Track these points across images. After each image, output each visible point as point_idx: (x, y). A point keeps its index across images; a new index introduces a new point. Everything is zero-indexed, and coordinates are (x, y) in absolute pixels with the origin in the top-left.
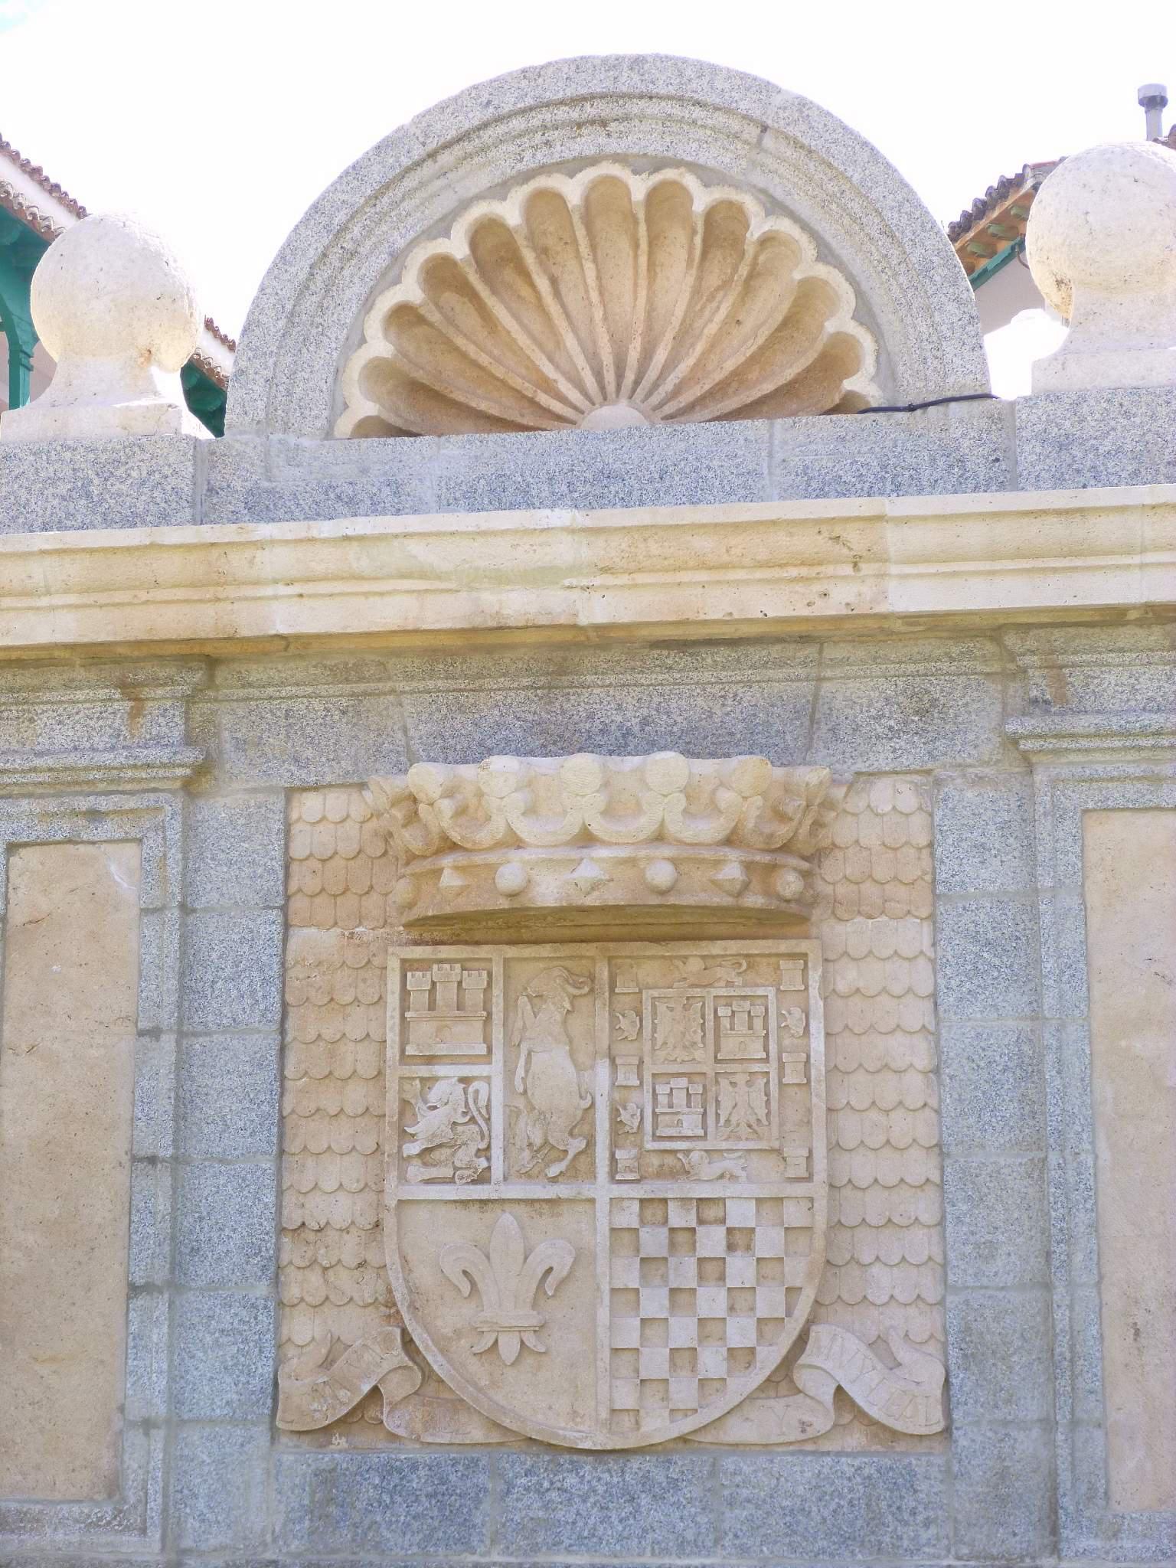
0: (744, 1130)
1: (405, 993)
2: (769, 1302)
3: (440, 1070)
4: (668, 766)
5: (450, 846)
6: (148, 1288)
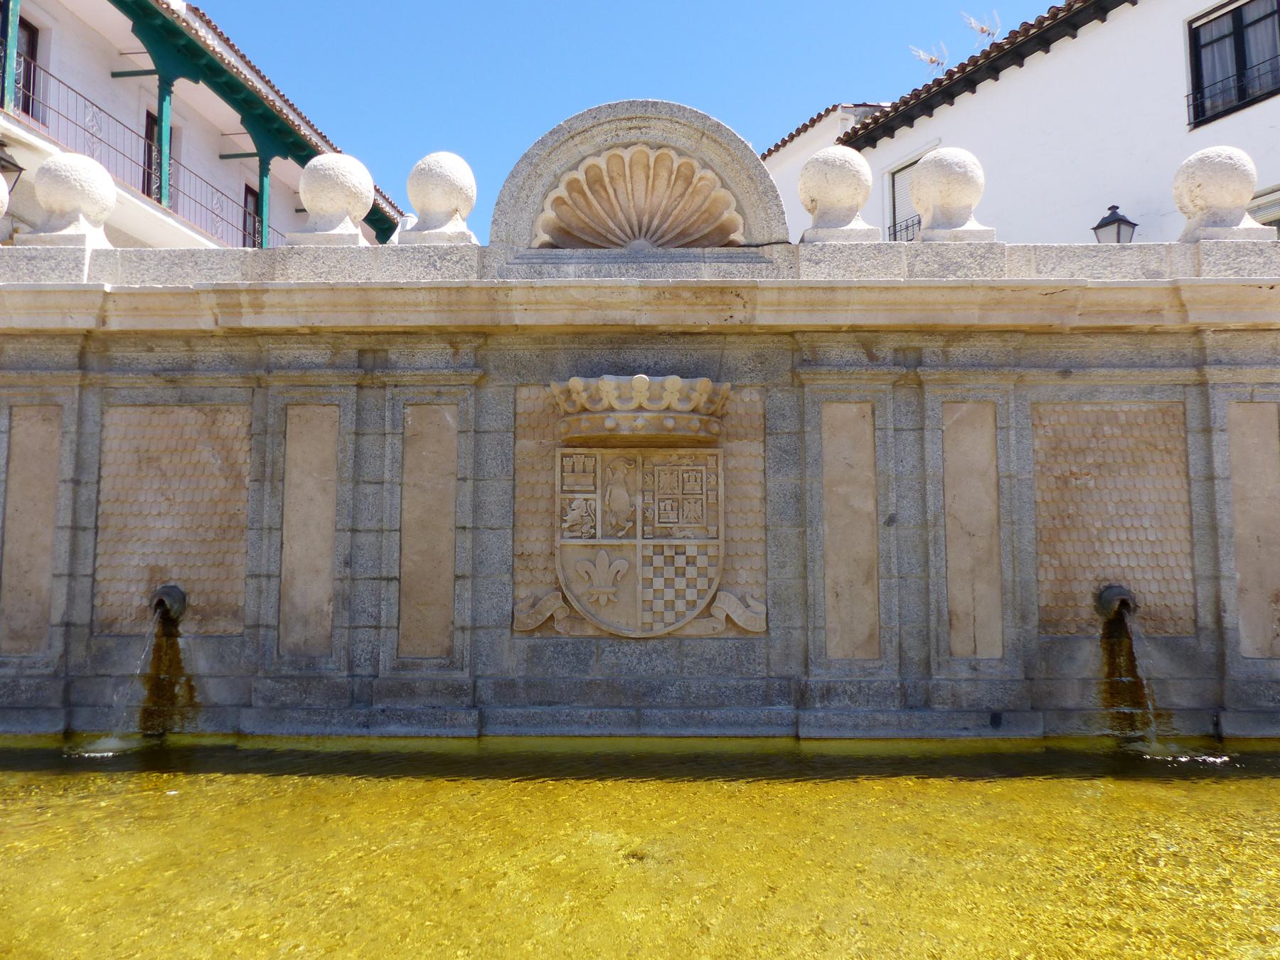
0: (693, 520)
1: (562, 466)
2: (702, 583)
3: (577, 496)
4: (673, 382)
5: (585, 410)
6: (463, 577)
